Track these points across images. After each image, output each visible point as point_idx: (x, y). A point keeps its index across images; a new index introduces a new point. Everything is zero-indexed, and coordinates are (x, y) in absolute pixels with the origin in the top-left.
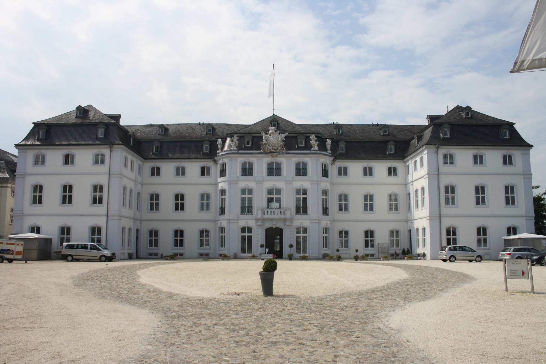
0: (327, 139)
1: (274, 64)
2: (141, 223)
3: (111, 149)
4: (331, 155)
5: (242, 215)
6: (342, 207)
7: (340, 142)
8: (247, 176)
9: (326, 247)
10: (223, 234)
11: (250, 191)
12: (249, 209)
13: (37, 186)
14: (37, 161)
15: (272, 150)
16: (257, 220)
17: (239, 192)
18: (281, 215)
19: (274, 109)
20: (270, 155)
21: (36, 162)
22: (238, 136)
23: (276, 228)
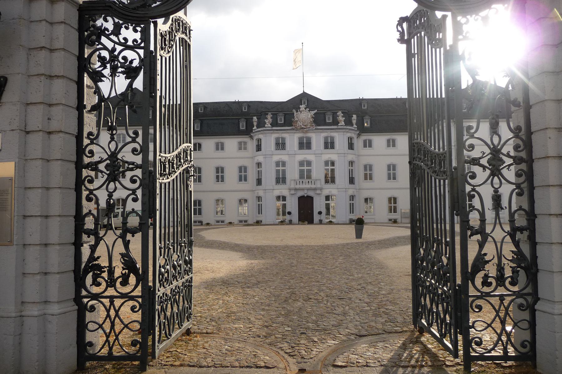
1: (302, 43)
4: (356, 129)
9: (353, 213)
10: (260, 169)
15: (303, 127)
16: (290, 189)
17: (274, 165)
18: (312, 184)
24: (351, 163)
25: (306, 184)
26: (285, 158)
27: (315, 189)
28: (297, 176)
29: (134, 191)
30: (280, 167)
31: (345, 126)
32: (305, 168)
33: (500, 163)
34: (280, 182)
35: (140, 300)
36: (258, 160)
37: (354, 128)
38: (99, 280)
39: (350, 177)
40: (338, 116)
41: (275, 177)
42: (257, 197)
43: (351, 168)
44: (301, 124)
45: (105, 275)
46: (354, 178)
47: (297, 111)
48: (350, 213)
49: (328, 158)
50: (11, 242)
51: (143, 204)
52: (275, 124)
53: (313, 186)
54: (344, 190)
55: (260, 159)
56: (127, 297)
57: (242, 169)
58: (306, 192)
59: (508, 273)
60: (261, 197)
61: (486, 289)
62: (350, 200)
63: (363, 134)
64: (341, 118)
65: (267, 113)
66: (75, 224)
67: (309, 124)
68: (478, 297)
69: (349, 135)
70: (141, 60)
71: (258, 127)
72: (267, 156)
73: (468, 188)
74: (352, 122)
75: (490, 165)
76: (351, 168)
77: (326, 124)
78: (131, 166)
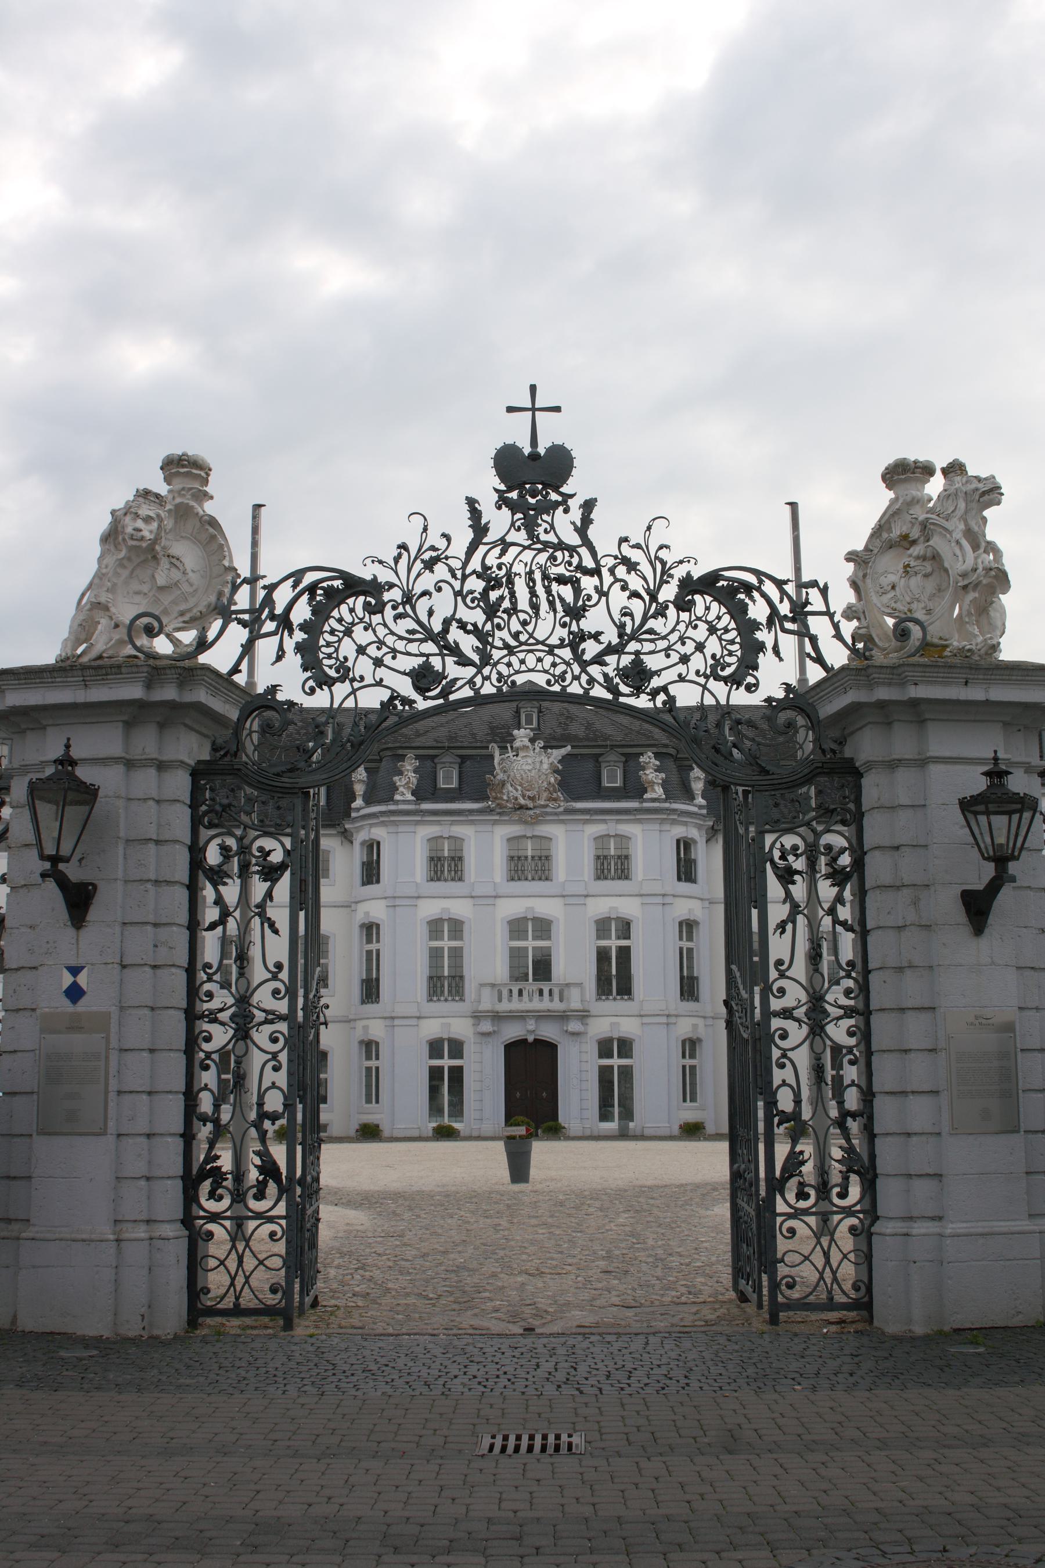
4: (704, 811)
9: (693, 1099)
10: (373, 947)
15: (522, 801)
16: (477, 1017)
17: (422, 932)
18: (551, 1001)
23: (537, 1041)
25: (531, 1000)
26: (460, 909)
27: (563, 1017)
28: (500, 970)
29: (275, 1056)
30: (442, 939)
31: (665, 801)
33: (821, 1016)
34: (442, 992)
35: (283, 1222)
36: (367, 914)
37: (695, 809)
38: (220, 1191)
39: (682, 978)
40: (644, 769)
41: (426, 973)
42: (361, 1042)
43: (686, 944)
44: (518, 794)
45: (229, 1183)
46: (697, 978)
47: (503, 749)
48: (685, 1100)
50: (103, 1133)
51: (290, 1074)
52: (427, 790)
53: (557, 1005)
54: (664, 1020)
55: (375, 910)
56: (264, 1217)
58: (531, 1027)
59: (835, 1178)
60: (377, 1044)
61: (802, 1204)
62: (684, 1056)
64: (652, 773)
65: (400, 752)
66: (185, 1105)
67: (545, 795)
68: (789, 1216)
69: (680, 831)
70: (287, 853)
71: (370, 799)
72: (398, 902)
73: (776, 1053)
74: (690, 786)
75: (809, 1019)
76: (686, 944)
77: (600, 793)
78: (270, 1017)
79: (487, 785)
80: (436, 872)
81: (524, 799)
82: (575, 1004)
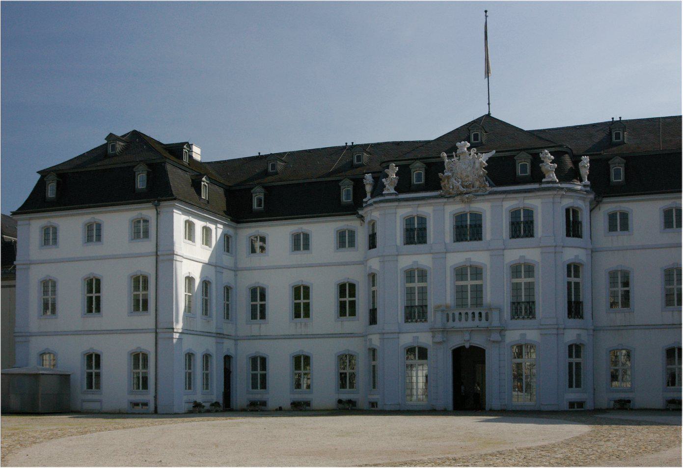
0: (581, 156)
1: (486, 11)
2: (236, 345)
3: (157, 210)
5: (407, 324)
6: (349, 308)
7: (611, 161)
8: (416, 244)
9: (578, 385)
10: (373, 289)
11: (423, 275)
12: (528, 307)
13: (92, 280)
14: (46, 238)
15: (462, 189)
16: (433, 331)
17: (400, 278)
18: (480, 320)
19: (489, 104)
20: (458, 198)
21: (45, 240)
22: (396, 166)
23: (472, 347)
24: (573, 269)
27: (488, 330)
28: (449, 298)
32: (523, 280)
39: (569, 302)
49: (573, 257)
55: (374, 264)
57: (346, 290)
63: (605, 200)
69: (567, 202)
76: (573, 280)
79: (439, 180)
80: (516, 232)
81: (463, 187)
82: (495, 322)
